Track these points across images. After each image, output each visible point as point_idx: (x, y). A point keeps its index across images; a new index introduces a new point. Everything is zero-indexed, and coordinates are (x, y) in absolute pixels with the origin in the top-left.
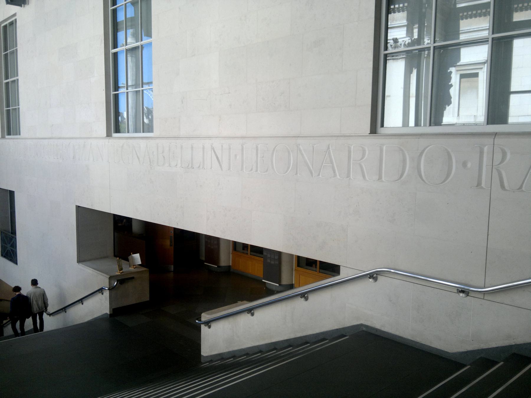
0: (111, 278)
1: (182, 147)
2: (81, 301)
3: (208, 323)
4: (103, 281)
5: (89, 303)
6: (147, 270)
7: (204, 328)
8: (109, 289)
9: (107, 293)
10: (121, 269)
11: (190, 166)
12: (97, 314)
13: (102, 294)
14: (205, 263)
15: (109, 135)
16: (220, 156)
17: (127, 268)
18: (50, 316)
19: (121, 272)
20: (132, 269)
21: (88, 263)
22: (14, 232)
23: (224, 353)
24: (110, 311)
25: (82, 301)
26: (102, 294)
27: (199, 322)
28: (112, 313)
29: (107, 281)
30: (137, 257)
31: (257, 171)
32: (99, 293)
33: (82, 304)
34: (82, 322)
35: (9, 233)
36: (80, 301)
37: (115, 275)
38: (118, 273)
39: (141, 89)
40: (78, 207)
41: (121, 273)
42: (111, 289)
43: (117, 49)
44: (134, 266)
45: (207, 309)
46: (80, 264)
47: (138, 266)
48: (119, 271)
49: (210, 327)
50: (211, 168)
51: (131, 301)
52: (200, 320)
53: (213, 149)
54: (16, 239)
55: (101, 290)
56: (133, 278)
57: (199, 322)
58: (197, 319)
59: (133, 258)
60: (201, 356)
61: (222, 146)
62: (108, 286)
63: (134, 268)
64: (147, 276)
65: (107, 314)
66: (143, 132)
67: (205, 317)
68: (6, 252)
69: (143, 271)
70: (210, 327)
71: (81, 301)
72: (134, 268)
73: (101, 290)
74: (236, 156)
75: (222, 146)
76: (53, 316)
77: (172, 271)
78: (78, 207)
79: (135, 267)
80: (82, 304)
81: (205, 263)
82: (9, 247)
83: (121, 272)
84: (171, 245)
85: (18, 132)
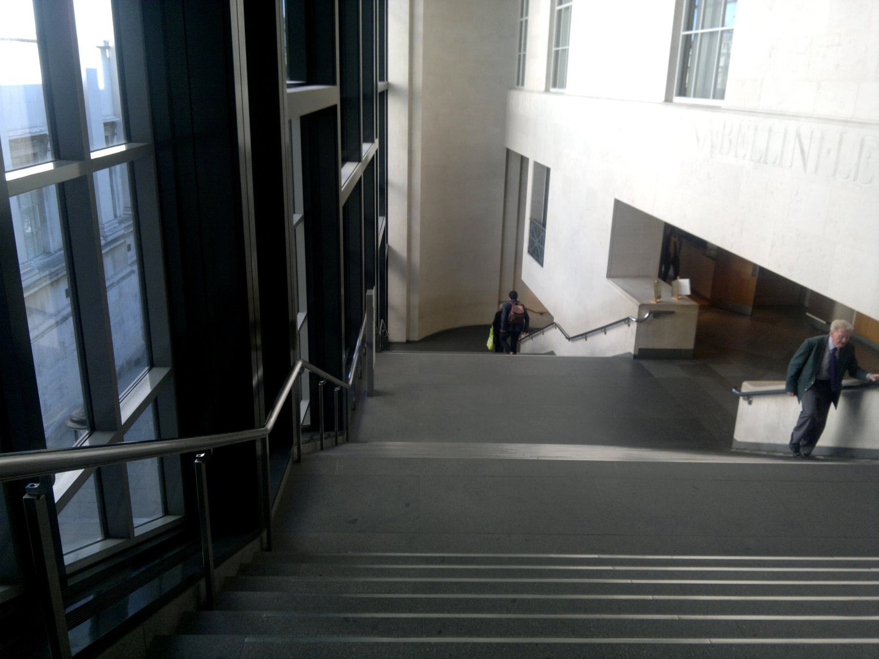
0: (642, 307)
1: (756, 129)
2: (604, 329)
3: (749, 397)
4: (629, 307)
5: (614, 335)
6: (693, 306)
7: (743, 403)
8: (637, 321)
9: (634, 326)
10: (658, 297)
11: (763, 159)
12: (620, 351)
13: (629, 325)
14: (808, 314)
15: (668, 99)
16: (806, 148)
17: (668, 297)
18: (569, 341)
19: (658, 300)
20: (674, 299)
21: (620, 281)
22: (544, 225)
23: (763, 444)
24: (635, 351)
25: (605, 330)
26: (629, 325)
27: (737, 392)
28: (637, 353)
29: (636, 310)
30: (685, 284)
31: (855, 179)
32: (625, 323)
33: (605, 333)
34: (602, 355)
35: (539, 225)
36: (603, 330)
37: (649, 303)
38: (653, 302)
39: (720, 29)
40: (618, 204)
41: (657, 302)
42: (640, 321)
43: (181, 453)
44: (679, 295)
45: (753, 377)
46: (610, 280)
47: (686, 297)
48: (655, 299)
49: (750, 403)
50: (791, 166)
51: (667, 343)
52: (739, 391)
53: (799, 136)
54: (545, 232)
55: (627, 321)
56: (672, 313)
57: (737, 392)
58: (736, 388)
59: (679, 285)
60: (732, 441)
61: (812, 133)
62: (637, 317)
63: (679, 299)
64: (695, 313)
65: (630, 353)
66: (714, 98)
67: (747, 387)
68: (533, 248)
69: (690, 306)
70: (750, 403)
71: (604, 329)
72: (679, 299)
73: (627, 321)
74: (829, 151)
75: (812, 133)
76: (572, 341)
77: (106, 240)
78: (618, 204)
79: (680, 297)
80: (605, 333)
81: (808, 314)
82: (537, 244)
83: (658, 300)
84: (753, 275)
85: (563, 86)
